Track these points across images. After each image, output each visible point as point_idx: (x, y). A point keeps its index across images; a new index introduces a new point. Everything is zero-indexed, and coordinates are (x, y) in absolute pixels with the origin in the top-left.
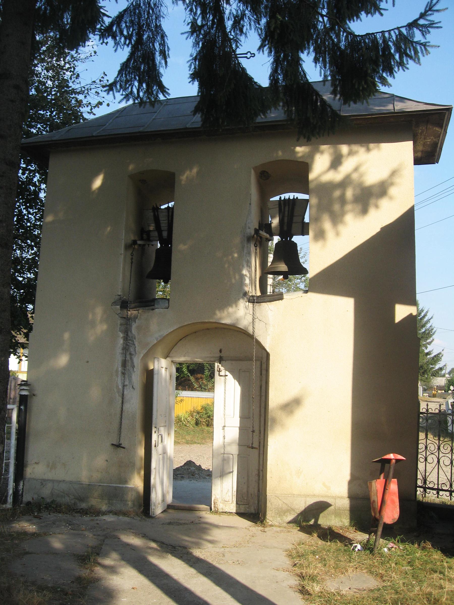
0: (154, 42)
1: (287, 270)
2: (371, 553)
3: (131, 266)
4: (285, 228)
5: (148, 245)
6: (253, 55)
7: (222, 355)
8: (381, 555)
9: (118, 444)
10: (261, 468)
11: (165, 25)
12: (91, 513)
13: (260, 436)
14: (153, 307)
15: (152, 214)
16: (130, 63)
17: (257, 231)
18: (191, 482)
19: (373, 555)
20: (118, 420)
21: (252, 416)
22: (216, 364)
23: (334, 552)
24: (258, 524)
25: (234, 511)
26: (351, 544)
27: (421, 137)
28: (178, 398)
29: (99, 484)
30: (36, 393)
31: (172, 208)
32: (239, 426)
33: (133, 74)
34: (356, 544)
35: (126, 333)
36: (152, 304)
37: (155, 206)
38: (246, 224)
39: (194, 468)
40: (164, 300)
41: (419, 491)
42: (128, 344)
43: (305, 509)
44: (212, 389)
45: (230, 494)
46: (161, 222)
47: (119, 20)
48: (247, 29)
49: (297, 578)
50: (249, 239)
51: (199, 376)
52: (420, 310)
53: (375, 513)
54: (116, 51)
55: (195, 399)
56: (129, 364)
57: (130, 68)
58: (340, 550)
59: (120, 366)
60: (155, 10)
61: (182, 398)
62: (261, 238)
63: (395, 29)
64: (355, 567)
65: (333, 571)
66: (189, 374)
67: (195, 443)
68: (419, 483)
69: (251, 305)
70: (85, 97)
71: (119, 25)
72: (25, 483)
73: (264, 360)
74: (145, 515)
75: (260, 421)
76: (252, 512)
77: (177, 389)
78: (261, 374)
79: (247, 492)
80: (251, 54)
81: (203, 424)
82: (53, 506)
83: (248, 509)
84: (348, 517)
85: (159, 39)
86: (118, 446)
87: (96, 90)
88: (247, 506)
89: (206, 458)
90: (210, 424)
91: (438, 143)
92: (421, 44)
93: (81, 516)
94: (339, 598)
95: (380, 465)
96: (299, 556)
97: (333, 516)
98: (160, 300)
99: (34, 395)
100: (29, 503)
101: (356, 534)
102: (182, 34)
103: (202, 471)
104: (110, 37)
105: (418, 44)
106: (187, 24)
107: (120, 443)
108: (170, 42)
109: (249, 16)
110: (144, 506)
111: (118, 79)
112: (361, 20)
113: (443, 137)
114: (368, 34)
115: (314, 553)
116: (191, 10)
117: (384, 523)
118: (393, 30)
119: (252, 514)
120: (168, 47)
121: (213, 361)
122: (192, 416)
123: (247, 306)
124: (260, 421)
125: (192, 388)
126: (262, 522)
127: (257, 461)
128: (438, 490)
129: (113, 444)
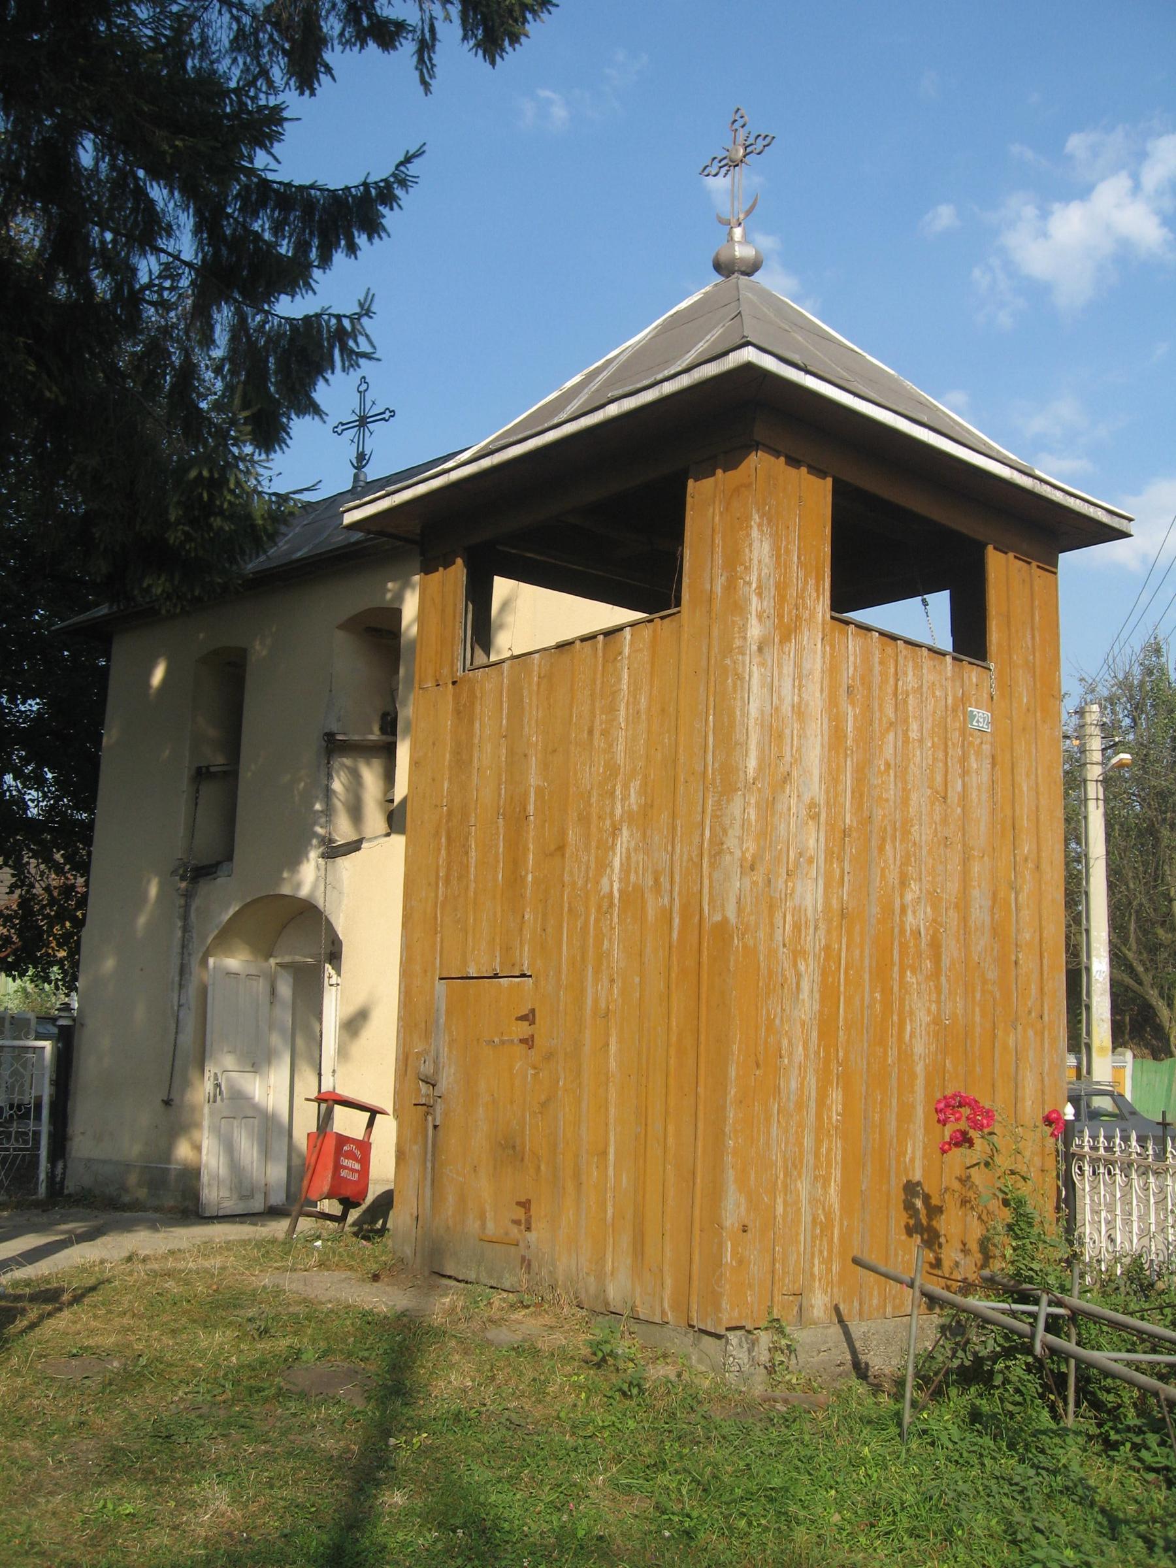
107: (171, 1097)
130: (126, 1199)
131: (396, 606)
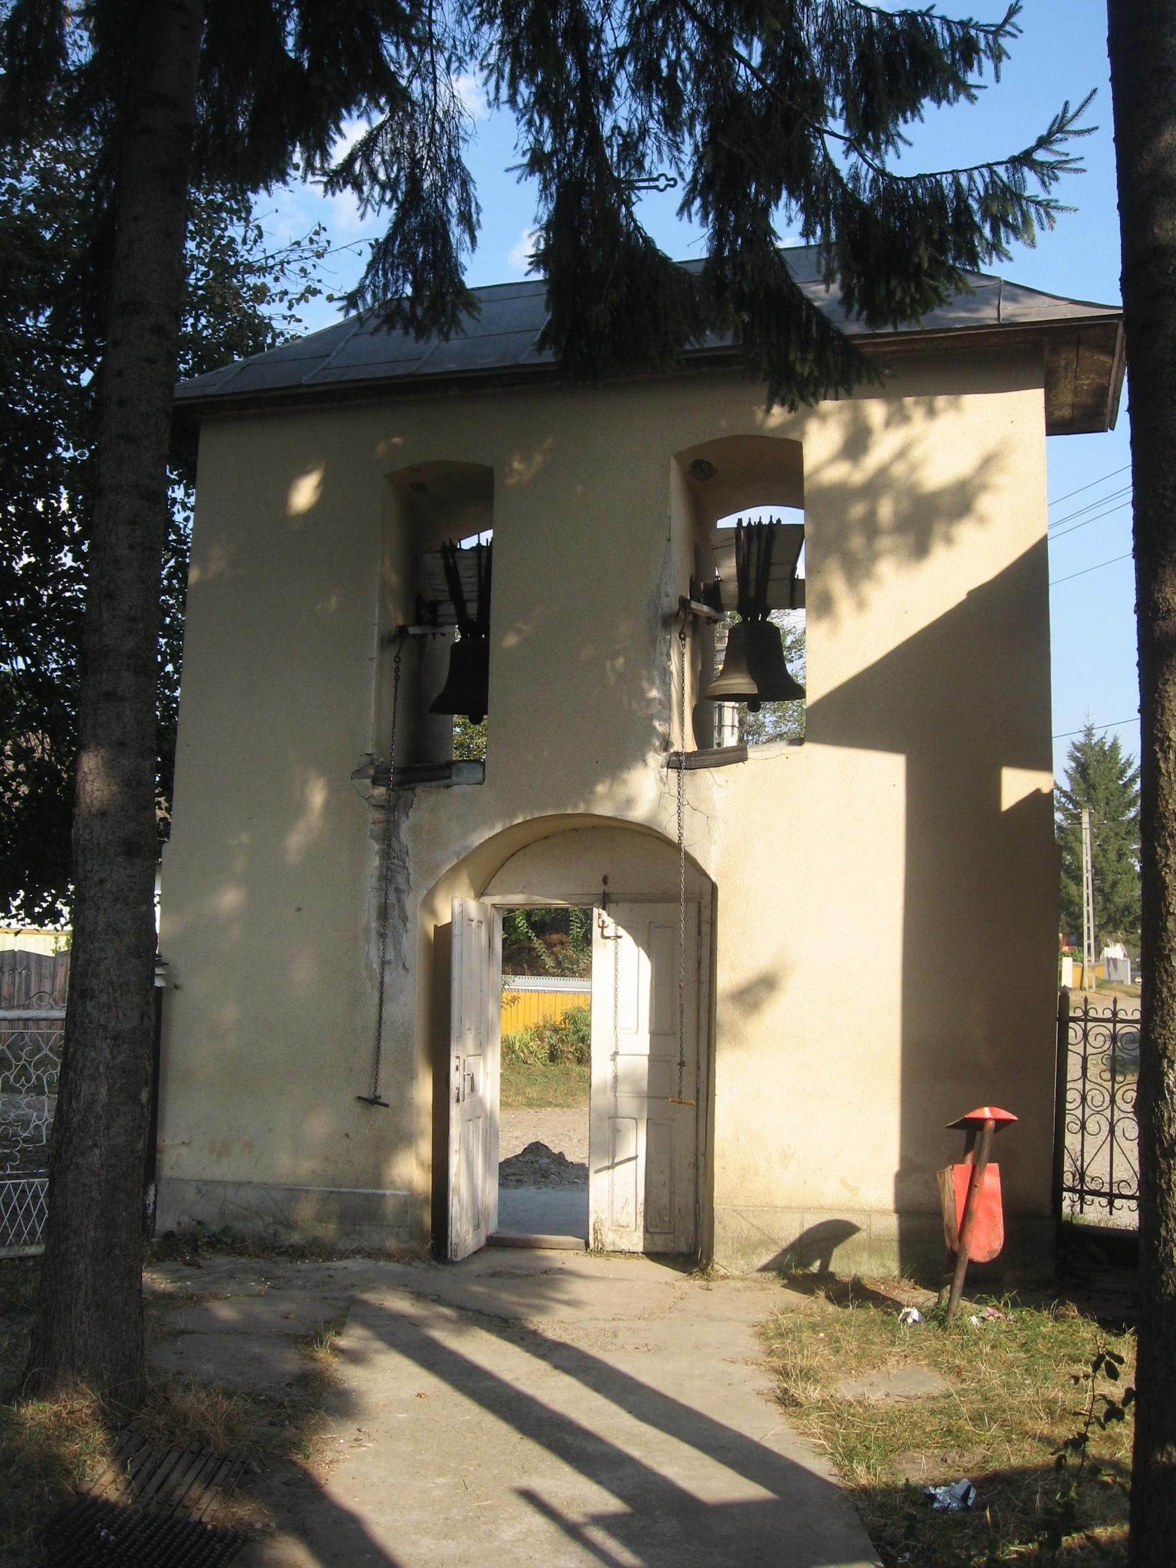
0: (446, 193)
1: (756, 692)
2: (939, 1327)
3: (396, 687)
4: (752, 592)
5: (434, 634)
6: (672, 183)
7: (610, 889)
8: (963, 1329)
9: (372, 1097)
10: (701, 1148)
11: (469, 157)
12: (313, 1254)
13: (698, 1076)
14: (447, 781)
15: (441, 562)
16: (394, 245)
17: (684, 603)
18: (541, 1191)
19: (945, 1329)
20: (371, 1043)
21: (678, 1027)
22: (596, 911)
23: (859, 1326)
24: (694, 1275)
25: (640, 1248)
26: (899, 1310)
27: (1067, 376)
28: (505, 994)
29: (329, 1189)
30: (179, 982)
31: (489, 548)
32: (648, 1052)
33: (401, 269)
34: (908, 1310)
35: (386, 842)
36: (446, 774)
37: (447, 544)
38: (659, 587)
39: (548, 1161)
40: (473, 765)
41: (1068, 1199)
42: (392, 866)
43: (801, 1237)
44: (586, 972)
45: (631, 1209)
46: (462, 580)
47: (367, 150)
48: (652, 162)
49: (774, 1377)
50: (667, 621)
51: (555, 937)
52: (1122, 762)
53: (952, 1241)
54: (362, 216)
55: (547, 995)
56: (395, 913)
57: (393, 256)
58: (873, 1321)
59: (374, 919)
60: (446, 124)
61: (515, 994)
62: (696, 616)
63: (983, 166)
64: (903, 1354)
65: (854, 1363)
66: (531, 934)
67: (550, 1104)
68: (1068, 1180)
69: (673, 774)
70: (277, 279)
71: (367, 160)
72: (160, 1189)
73: (707, 899)
74: (436, 1260)
75: (698, 1041)
76: (682, 1250)
77: (504, 972)
78: (699, 933)
79: (670, 1204)
80: (668, 180)
81: (568, 1059)
82: (225, 1240)
83: (672, 1244)
84: (897, 1258)
85: (456, 187)
86: (373, 1101)
87: (301, 264)
88: (669, 1237)
89: (575, 1141)
90: (583, 1058)
91: (1108, 387)
92: (1038, 203)
93: (291, 1262)
94: (861, 1410)
95: (965, 1136)
96: (781, 1335)
97: (865, 1255)
98: (464, 764)
99: (177, 987)
100: (169, 1235)
101: (916, 1293)
102: (508, 170)
103: (567, 1167)
104: (349, 187)
105: (1032, 202)
106: (520, 153)
107: (377, 1094)
108: (481, 193)
109: (655, 134)
110: (433, 1239)
111: (367, 282)
112: (922, 120)
113: (1117, 373)
114: (920, 177)
115: (814, 1327)
116: (530, 123)
117: (971, 1262)
118: (976, 168)
119: (681, 1254)
120: (477, 203)
121: (588, 904)
122: (541, 1039)
123: (664, 778)
124: (698, 1041)
125: (537, 969)
126: (703, 1270)
127: (693, 1134)
128: (1111, 1197)
129: (360, 1098)
130: (296, 1238)
131: (793, 436)
